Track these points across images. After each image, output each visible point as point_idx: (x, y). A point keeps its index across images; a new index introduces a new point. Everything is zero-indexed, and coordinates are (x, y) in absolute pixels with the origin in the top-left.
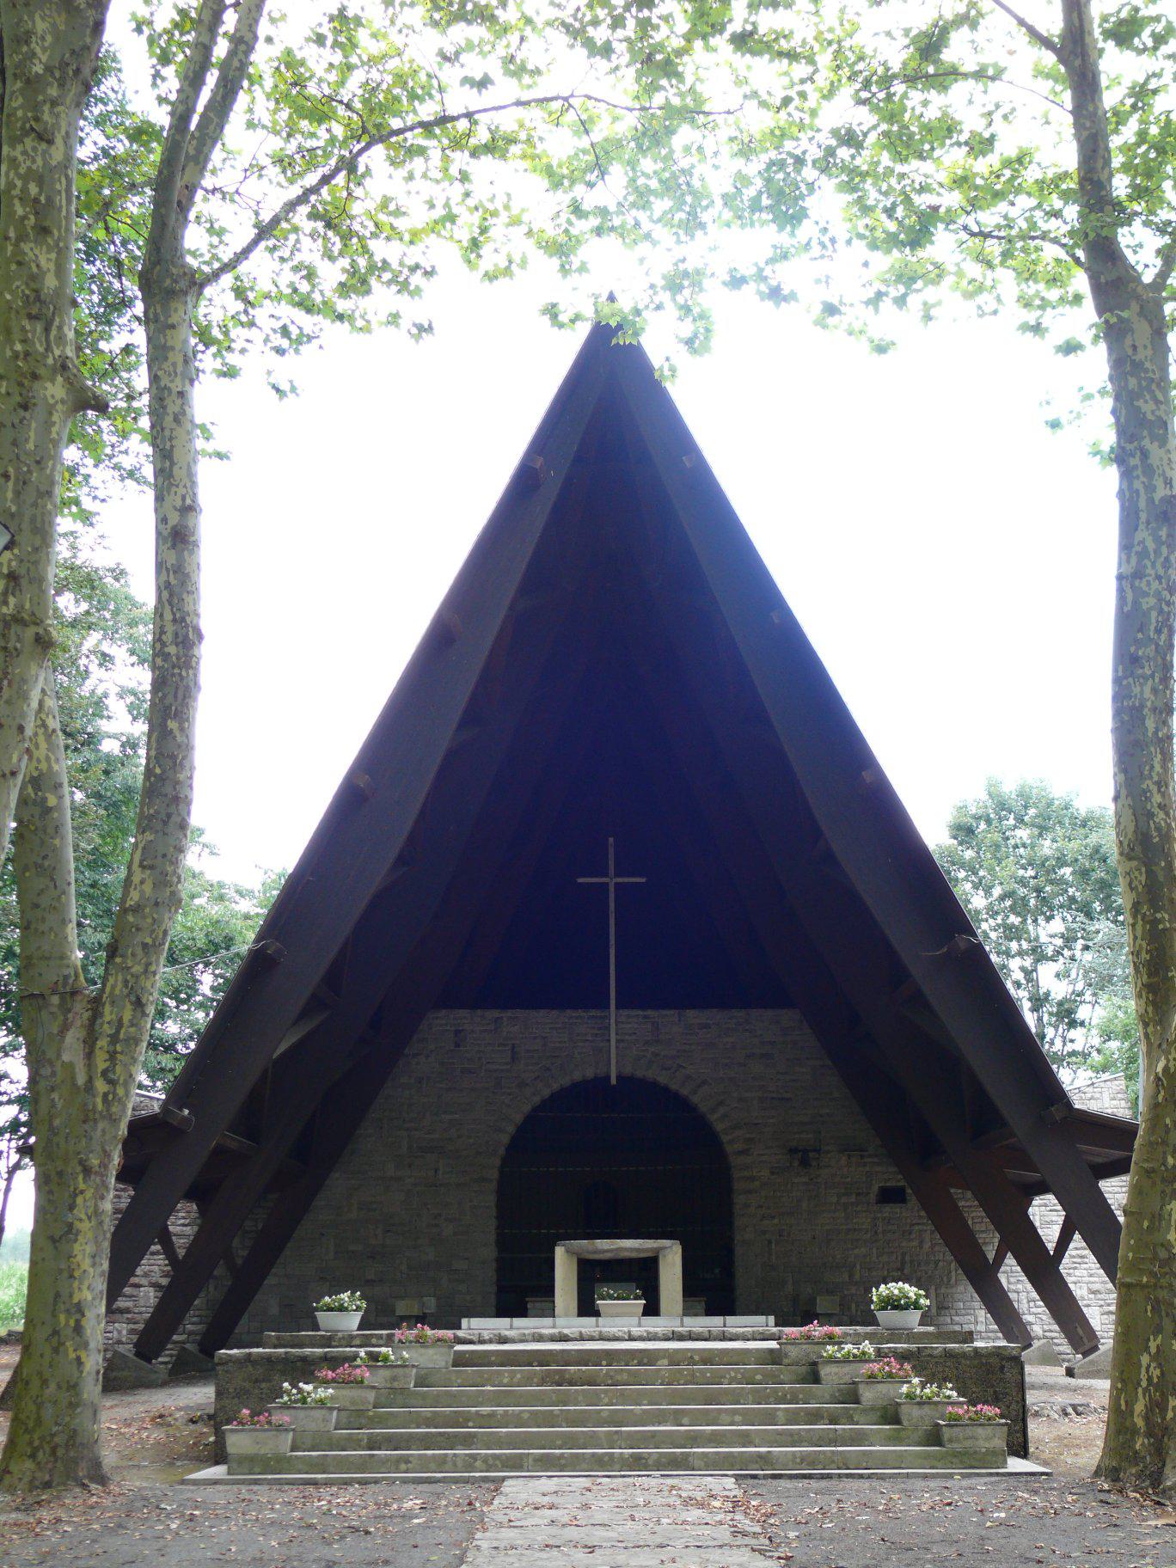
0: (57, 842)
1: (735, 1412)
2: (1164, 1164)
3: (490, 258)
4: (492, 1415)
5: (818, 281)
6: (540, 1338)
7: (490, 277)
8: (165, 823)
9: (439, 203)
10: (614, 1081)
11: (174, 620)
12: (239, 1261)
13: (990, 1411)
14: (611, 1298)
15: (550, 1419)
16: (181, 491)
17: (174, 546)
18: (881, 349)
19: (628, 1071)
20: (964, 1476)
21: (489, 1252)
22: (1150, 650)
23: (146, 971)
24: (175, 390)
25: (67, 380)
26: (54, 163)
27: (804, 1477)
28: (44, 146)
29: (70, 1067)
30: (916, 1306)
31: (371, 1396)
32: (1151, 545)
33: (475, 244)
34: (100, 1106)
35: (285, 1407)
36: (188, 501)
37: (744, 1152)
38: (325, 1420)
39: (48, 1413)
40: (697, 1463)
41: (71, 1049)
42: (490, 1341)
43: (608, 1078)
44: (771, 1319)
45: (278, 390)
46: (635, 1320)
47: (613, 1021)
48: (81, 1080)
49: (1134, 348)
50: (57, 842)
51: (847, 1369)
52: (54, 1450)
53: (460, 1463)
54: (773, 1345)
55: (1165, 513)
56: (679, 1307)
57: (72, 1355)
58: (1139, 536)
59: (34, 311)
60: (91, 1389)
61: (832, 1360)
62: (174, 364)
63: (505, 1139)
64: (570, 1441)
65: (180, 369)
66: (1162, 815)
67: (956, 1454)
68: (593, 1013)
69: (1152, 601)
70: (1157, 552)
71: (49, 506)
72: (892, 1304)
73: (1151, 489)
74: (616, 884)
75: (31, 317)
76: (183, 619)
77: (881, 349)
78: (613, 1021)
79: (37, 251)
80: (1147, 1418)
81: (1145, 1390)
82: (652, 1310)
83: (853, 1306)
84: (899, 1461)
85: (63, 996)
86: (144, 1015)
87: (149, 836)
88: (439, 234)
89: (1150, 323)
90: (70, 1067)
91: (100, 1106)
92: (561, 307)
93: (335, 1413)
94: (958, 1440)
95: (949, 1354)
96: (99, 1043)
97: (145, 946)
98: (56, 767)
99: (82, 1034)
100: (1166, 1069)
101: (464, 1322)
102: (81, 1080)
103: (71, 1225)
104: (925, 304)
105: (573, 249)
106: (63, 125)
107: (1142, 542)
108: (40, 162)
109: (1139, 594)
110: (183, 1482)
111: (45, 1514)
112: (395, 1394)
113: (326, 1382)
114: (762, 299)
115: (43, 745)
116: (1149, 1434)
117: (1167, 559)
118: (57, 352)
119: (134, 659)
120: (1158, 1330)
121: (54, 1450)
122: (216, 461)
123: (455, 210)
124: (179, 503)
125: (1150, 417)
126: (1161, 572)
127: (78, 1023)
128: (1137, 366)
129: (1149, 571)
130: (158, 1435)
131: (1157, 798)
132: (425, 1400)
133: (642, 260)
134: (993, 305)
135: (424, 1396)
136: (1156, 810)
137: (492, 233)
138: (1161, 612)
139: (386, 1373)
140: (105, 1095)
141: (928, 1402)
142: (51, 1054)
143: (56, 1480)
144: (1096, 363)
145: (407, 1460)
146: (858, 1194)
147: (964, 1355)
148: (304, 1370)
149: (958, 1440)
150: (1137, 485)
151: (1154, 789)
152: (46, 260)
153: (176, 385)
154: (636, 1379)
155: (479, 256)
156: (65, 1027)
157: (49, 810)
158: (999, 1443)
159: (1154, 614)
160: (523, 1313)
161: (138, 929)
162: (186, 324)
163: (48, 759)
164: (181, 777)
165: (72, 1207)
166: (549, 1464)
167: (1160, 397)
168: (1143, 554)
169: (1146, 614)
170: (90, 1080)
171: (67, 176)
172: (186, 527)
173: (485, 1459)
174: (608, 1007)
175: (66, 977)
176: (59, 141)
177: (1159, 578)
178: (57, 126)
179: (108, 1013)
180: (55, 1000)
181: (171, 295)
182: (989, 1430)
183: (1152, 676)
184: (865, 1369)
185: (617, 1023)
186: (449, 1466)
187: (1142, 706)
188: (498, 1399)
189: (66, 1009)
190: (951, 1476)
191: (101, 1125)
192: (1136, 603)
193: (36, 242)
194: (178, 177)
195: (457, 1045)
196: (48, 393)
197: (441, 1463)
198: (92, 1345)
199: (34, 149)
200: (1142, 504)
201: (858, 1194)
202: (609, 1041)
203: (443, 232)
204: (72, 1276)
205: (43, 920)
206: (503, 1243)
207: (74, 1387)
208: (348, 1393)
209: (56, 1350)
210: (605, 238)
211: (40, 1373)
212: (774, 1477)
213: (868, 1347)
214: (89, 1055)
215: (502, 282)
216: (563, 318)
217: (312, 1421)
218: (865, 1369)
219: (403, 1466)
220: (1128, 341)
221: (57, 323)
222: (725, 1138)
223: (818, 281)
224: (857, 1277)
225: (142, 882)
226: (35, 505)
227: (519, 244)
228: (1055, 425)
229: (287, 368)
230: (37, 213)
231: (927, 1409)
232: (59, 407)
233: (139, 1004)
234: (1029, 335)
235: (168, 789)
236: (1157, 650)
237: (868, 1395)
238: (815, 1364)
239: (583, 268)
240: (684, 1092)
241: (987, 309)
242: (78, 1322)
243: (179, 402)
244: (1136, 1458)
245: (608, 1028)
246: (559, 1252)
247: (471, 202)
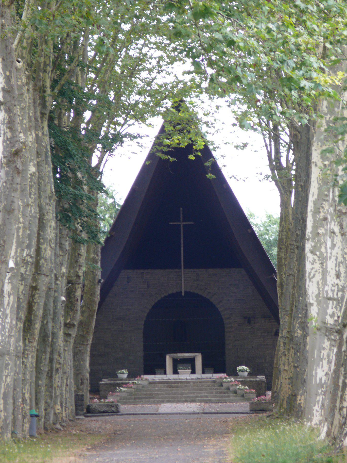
4: (158, 394)
10: (183, 294)
14: (182, 369)
19: (188, 290)
21: (141, 353)
30: (246, 371)
37: (228, 318)
43: (181, 292)
51: (228, 384)
61: (225, 382)
63: (146, 314)
67: (246, 399)
68: (176, 270)
72: (241, 371)
74: (183, 225)
78: (183, 272)
82: (193, 372)
83: (266, 370)
95: (251, 381)
109: (282, 235)
112: (138, 390)
114: (212, 142)
141: (242, 389)
146: (268, 332)
147: (254, 381)
148: (119, 385)
151: (283, 274)
154: (186, 386)
160: (154, 373)
168: (283, 227)
169: (283, 239)
174: (180, 268)
184: (231, 384)
185: (184, 273)
192: (282, 237)
195: (128, 282)
201: (268, 332)
202: (181, 280)
206: (145, 348)
218: (231, 384)
224: (267, 360)
231: (242, 391)
237: (231, 388)
240: (208, 297)
245: (181, 276)
246: (168, 357)
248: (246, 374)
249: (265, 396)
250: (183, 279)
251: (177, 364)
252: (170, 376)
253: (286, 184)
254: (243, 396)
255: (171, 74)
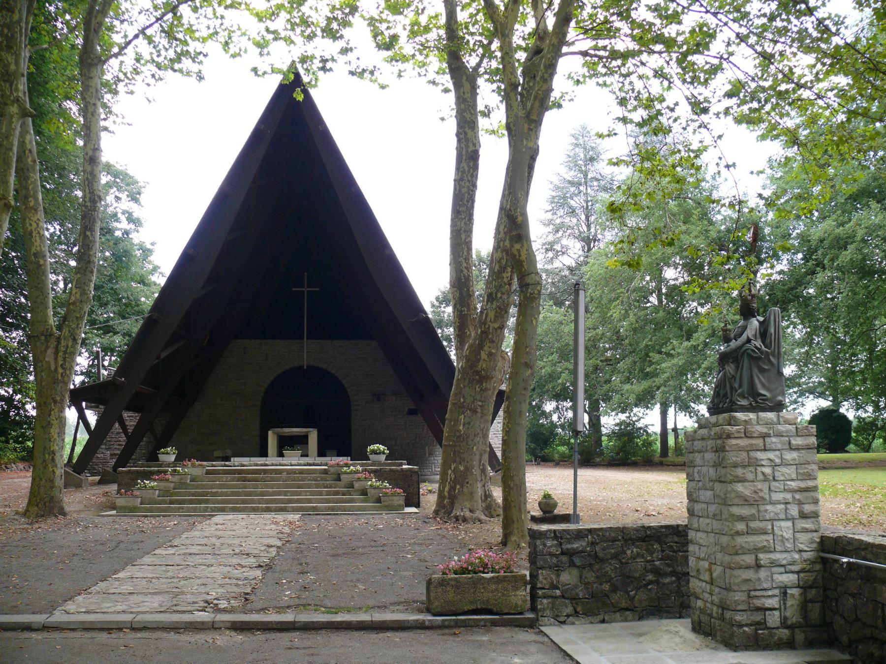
0: (43, 278)
1: (307, 491)
2: (460, 401)
3: (233, 49)
4: (217, 492)
5: (346, 63)
6: (257, 465)
7: (233, 56)
8: (85, 271)
9: (212, 27)
10: (305, 367)
11: (90, 193)
12: (159, 436)
13: (399, 490)
15: (238, 494)
16: (94, 142)
17: (90, 164)
18: (383, 87)
20: (386, 514)
22: (464, 208)
23: (77, 327)
24: (92, 103)
25: (19, 106)
26: (14, 20)
27: (328, 514)
28: (10, 14)
29: (48, 363)
30: (384, 453)
31: (172, 485)
32: (466, 169)
33: (227, 43)
34: (60, 378)
35: (139, 489)
36: (96, 146)
38: (153, 494)
39: (42, 490)
40: (290, 510)
41: (49, 356)
42: (238, 466)
44: (349, 458)
45: (149, 100)
46: (297, 458)
47: (305, 344)
48: (53, 368)
49: (464, 93)
50: (43, 278)
51: (350, 476)
52: (45, 503)
53: (202, 509)
54: (326, 467)
55: (472, 156)
56: (316, 454)
57: (51, 470)
58: (462, 165)
59: (6, 79)
60: (60, 482)
61: (346, 473)
62: (92, 93)
64: (244, 502)
65: (94, 94)
66: (466, 271)
67: (386, 506)
69: (466, 190)
70: (469, 171)
71: (11, 154)
72: (374, 452)
73: (467, 147)
74: (308, 292)
75: (4, 81)
76: (93, 192)
77: (383, 87)
78: (305, 344)
79: (7, 55)
80: (449, 492)
81: (449, 483)
84: (364, 509)
85: (46, 336)
86: (77, 343)
87: (79, 276)
88: (212, 39)
89: (470, 84)
90: (48, 363)
91: (60, 378)
92: (259, 69)
93: (157, 491)
94: (386, 501)
95: (391, 470)
96: (60, 354)
97: (77, 317)
98: (43, 249)
99: (53, 351)
100: (462, 366)
101: (232, 459)
102: (53, 368)
103: (49, 422)
104: (400, 70)
105: (267, 46)
106: (19, 5)
107: (463, 167)
108: (8, 20)
110: (99, 516)
111: (37, 525)
112: (182, 485)
113: (155, 480)
115: (38, 240)
116: (449, 498)
117: (472, 174)
118: (15, 95)
119: (130, 199)
120: (455, 462)
121: (45, 503)
122: (127, 126)
123: (218, 30)
124: (92, 147)
125: (468, 119)
126: (470, 179)
127: (52, 346)
128: (465, 100)
129: (465, 178)
130: (103, 499)
131: (465, 265)
132: (193, 487)
133: (290, 52)
134: (424, 73)
135: (193, 485)
136: (464, 269)
137: (233, 39)
138: (469, 194)
139: (179, 477)
140: (62, 373)
141: (378, 488)
142: (41, 358)
143: (46, 514)
144: (451, 97)
145: (182, 508)
147: (397, 471)
148: (147, 476)
149: (386, 501)
150: (463, 145)
151: (464, 261)
152: (11, 59)
153: (92, 101)
155: (229, 48)
156: (47, 348)
157: (41, 266)
158: (402, 502)
159: (466, 195)
161: (74, 311)
162: (97, 77)
163: (40, 246)
164: (91, 253)
165: (50, 415)
166: (234, 510)
167: (473, 112)
169: (463, 195)
170: (56, 368)
171: (20, 26)
172: (95, 156)
173: (211, 508)
174: (303, 339)
175: (47, 329)
176: (17, 12)
177: (469, 181)
178: (16, 6)
179: (63, 343)
180: (43, 338)
181: (91, 65)
182: (398, 497)
183: (465, 218)
184: (357, 476)
186: (198, 510)
187: (460, 230)
188: (220, 487)
189: (47, 341)
190: (382, 514)
191: (60, 385)
192: (460, 191)
193: (7, 51)
194: (93, 19)
195: (245, 353)
196: (11, 111)
197: (195, 510)
198: (59, 466)
199: (6, 15)
200: (464, 152)
203: (214, 39)
204: (50, 441)
205: (38, 307)
207: (52, 481)
208: (163, 484)
209: (45, 468)
210: (278, 42)
211: (39, 476)
212: (316, 514)
213: (359, 468)
214: (56, 359)
215: (238, 58)
216: (260, 73)
217: (148, 494)
218: (357, 476)
219: (181, 510)
220: (462, 90)
221: (15, 83)
222: (348, 390)
223: (346, 63)
225: (76, 293)
226: (5, 153)
227: (244, 43)
228: (443, 119)
229: (151, 92)
230: (7, 41)
232: (16, 116)
233: (75, 340)
234: (431, 85)
235: (86, 258)
236: (467, 209)
237: (357, 485)
238: (339, 474)
239: (268, 54)
240: (333, 372)
241: (422, 74)
242: (53, 457)
243: (93, 107)
244: (444, 507)
245: (303, 347)
246: (270, 433)
247: (223, 27)
248: (382, 458)
249: (569, 567)
250: (305, 353)
251: (285, 444)
252: (272, 461)
253: (469, 95)
254: (379, 500)
255: (272, 29)
